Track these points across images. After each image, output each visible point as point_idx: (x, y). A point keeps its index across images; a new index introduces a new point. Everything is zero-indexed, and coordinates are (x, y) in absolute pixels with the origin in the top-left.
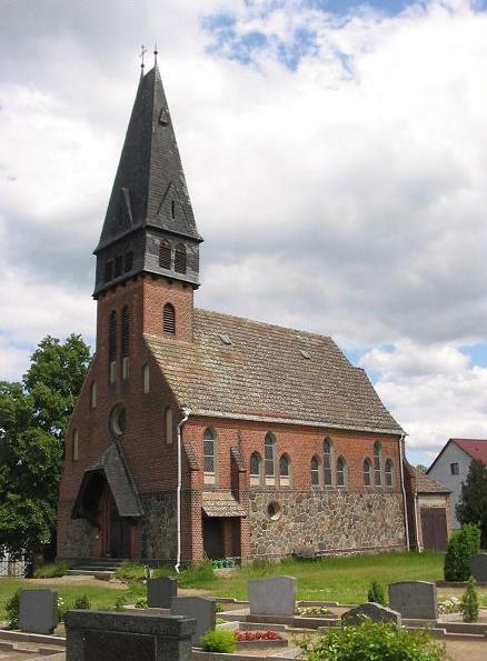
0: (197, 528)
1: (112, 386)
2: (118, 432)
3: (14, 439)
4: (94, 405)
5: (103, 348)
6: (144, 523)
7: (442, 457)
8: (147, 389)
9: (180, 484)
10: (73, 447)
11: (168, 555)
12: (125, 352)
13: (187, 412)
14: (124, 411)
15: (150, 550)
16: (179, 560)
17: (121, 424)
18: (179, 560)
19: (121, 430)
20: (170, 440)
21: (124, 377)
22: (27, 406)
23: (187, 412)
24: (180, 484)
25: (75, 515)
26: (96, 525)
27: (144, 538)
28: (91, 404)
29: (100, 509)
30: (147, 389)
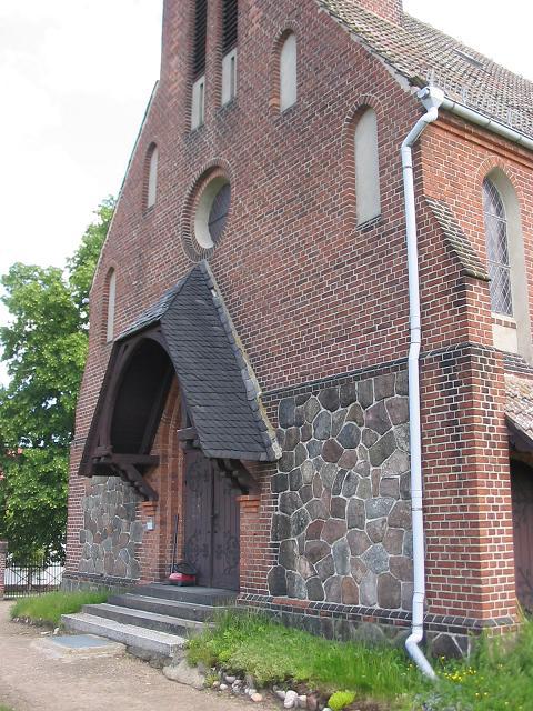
0: (494, 491)
1: (191, 136)
2: (205, 242)
3: (39, 353)
4: (151, 201)
5: (175, 61)
6: (280, 485)
7: (216, 507)
8: (288, 96)
9: (416, 336)
10: (105, 311)
11: (369, 594)
12: (230, 38)
13: (438, 96)
14: (226, 186)
15: (302, 569)
16: (418, 618)
17: (215, 225)
18: (418, 618)
19: (215, 236)
20: (368, 206)
21: (226, 98)
22: (62, 297)
23: (438, 96)
24: (416, 336)
25: (95, 467)
26: (146, 494)
27: (282, 528)
28: (145, 201)
29: (156, 451)
30: (288, 96)
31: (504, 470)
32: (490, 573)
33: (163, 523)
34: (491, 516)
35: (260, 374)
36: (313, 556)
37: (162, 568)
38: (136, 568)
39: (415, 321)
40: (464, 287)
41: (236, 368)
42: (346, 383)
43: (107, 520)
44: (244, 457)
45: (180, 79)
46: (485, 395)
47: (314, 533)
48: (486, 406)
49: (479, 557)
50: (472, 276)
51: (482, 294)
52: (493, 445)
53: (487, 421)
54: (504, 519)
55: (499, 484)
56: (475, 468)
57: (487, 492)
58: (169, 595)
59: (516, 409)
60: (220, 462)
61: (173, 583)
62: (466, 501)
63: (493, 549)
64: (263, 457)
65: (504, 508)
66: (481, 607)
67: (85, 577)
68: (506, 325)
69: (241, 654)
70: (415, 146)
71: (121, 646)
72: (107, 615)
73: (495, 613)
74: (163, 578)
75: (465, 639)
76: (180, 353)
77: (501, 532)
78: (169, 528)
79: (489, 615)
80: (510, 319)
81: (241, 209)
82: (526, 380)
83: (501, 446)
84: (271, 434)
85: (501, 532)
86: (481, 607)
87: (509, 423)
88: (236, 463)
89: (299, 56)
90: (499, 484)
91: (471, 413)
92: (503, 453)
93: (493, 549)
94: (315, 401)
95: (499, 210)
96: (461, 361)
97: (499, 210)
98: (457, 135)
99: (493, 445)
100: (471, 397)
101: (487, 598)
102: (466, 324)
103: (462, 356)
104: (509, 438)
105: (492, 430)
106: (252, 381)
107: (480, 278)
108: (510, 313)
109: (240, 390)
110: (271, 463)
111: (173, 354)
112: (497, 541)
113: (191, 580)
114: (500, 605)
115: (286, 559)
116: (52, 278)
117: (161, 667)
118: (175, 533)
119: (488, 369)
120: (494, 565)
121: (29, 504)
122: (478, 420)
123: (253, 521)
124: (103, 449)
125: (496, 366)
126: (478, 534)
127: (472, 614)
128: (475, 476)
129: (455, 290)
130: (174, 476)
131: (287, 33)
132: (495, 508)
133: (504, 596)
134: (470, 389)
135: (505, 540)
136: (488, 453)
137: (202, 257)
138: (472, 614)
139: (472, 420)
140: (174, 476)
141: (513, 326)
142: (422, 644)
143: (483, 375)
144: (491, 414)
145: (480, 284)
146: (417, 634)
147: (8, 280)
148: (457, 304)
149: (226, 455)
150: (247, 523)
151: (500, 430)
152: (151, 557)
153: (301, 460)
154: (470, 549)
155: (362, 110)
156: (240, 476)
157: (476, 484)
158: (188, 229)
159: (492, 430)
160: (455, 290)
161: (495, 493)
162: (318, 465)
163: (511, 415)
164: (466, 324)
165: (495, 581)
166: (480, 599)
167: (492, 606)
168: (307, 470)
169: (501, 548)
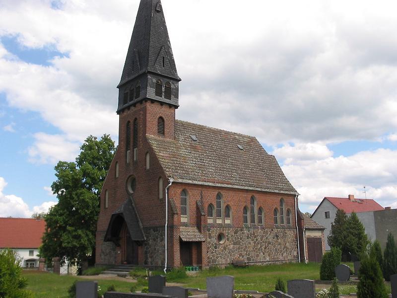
2: (131, 191)
3: (71, 195)
6: (146, 245)
8: (148, 167)
9: (167, 222)
12: (135, 146)
13: (171, 180)
15: (150, 260)
16: (166, 266)
18: (166, 266)
20: (161, 197)
23: (171, 180)
24: (167, 222)
26: (118, 245)
30: (148, 167)
33: (122, 252)
35: (142, 223)
36: (151, 257)
37: (122, 261)
38: (115, 262)
39: (167, 220)
41: (138, 221)
42: (157, 227)
43: (108, 251)
44: (139, 240)
45: (124, 149)
47: (151, 253)
58: (124, 266)
60: (135, 241)
61: (125, 264)
64: (143, 240)
67: (102, 265)
69: (139, 273)
70: (168, 189)
71: (116, 275)
72: (112, 270)
74: (122, 263)
75: (145, 264)
76: (127, 219)
78: (123, 252)
80: (186, 216)
81: (138, 188)
84: (144, 235)
88: (138, 241)
89: (150, 156)
94: (152, 230)
106: (141, 224)
109: (139, 226)
110: (144, 241)
111: (125, 219)
113: (129, 263)
115: (147, 258)
116: (72, 167)
117: (125, 277)
118: (124, 254)
121: (70, 245)
123: (140, 251)
124: (109, 237)
130: (124, 242)
131: (147, 152)
137: (130, 195)
140: (124, 242)
142: (166, 270)
146: (166, 269)
147: (56, 168)
149: (136, 240)
150: (140, 252)
152: (119, 259)
153: (149, 240)
155: (160, 178)
156: (140, 243)
158: (127, 187)
162: (152, 242)
168: (150, 242)
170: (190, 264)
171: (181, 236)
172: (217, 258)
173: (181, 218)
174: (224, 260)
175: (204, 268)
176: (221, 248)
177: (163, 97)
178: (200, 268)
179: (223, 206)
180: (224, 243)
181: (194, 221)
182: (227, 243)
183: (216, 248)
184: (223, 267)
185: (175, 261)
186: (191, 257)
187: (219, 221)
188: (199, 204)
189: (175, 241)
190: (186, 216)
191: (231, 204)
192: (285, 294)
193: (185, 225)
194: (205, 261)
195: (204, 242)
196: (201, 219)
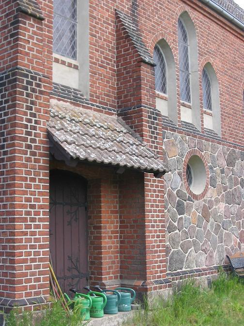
31: (44, 175)
32: (25, 261)
34: (28, 213)
40: (18, 22)
46: (29, 112)
48: (29, 121)
49: (14, 248)
50: (26, 13)
51: (35, 29)
52: (33, 154)
53: (29, 133)
54: (41, 216)
55: (37, 187)
56: (14, 172)
57: (25, 193)
59: (59, 126)
62: (7, 200)
63: (29, 240)
65: (41, 207)
66: (14, 289)
68: (70, 65)
73: (28, 294)
77: (37, 227)
79: (21, 295)
80: (73, 62)
82: (81, 109)
83: (41, 155)
85: (37, 227)
86: (14, 289)
87: (49, 136)
90: (37, 187)
91: (14, 125)
92: (43, 161)
93: (29, 240)
95: (185, 38)
96: (10, 82)
97: (185, 38)
98: (222, 26)
99: (33, 154)
100: (14, 112)
101: (21, 282)
102: (17, 52)
103: (11, 78)
104: (49, 149)
105: (33, 141)
107: (34, 16)
108: (74, 56)
112: (33, 234)
114: (33, 287)
119: (33, 90)
120: (29, 254)
122: (20, 132)
125: (43, 89)
126: (14, 227)
127: (9, 296)
128: (14, 179)
129: (12, 24)
132: (33, 207)
133: (38, 280)
134: (14, 106)
135: (41, 233)
136: (28, 160)
138: (9, 296)
139: (14, 132)
141: (76, 67)
143: (28, 95)
144: (34, 128)
145: (34, 21)
148: (12, 36)
151: (41, 142)
154: (8, 241)
157: (14, 185)
159: (33, 141)
160: (12, 24)
161: (33, 193)
163: (52, 131)
164: (17, 52)
165: (29, 268)
166: (13, 282)
167: (25, 288)
169: (37, 240)
170: (95, 286)
171: (59, 136)
172: (185, 248)
173: (55, 66)
174: (203, 258)
175: (153, 298)
176: (195, 209)
177: (28, 208)
178: (141, 296)
179: (196, 64)
180: (203, 195)
181: (107, 87)
182: (212, 194)
183: (181, 209)
184: (203, 280)
185: (20, 269)
186: (94, 245)
187: (187, 116)
188: (128, 22)
189: (21, 158)
190: (73, 62)
191: (217, 63)
192: (177, 271)
193: (65, 93)
194: (155, 263)
195: (158, 174)
196: (139, 78)
